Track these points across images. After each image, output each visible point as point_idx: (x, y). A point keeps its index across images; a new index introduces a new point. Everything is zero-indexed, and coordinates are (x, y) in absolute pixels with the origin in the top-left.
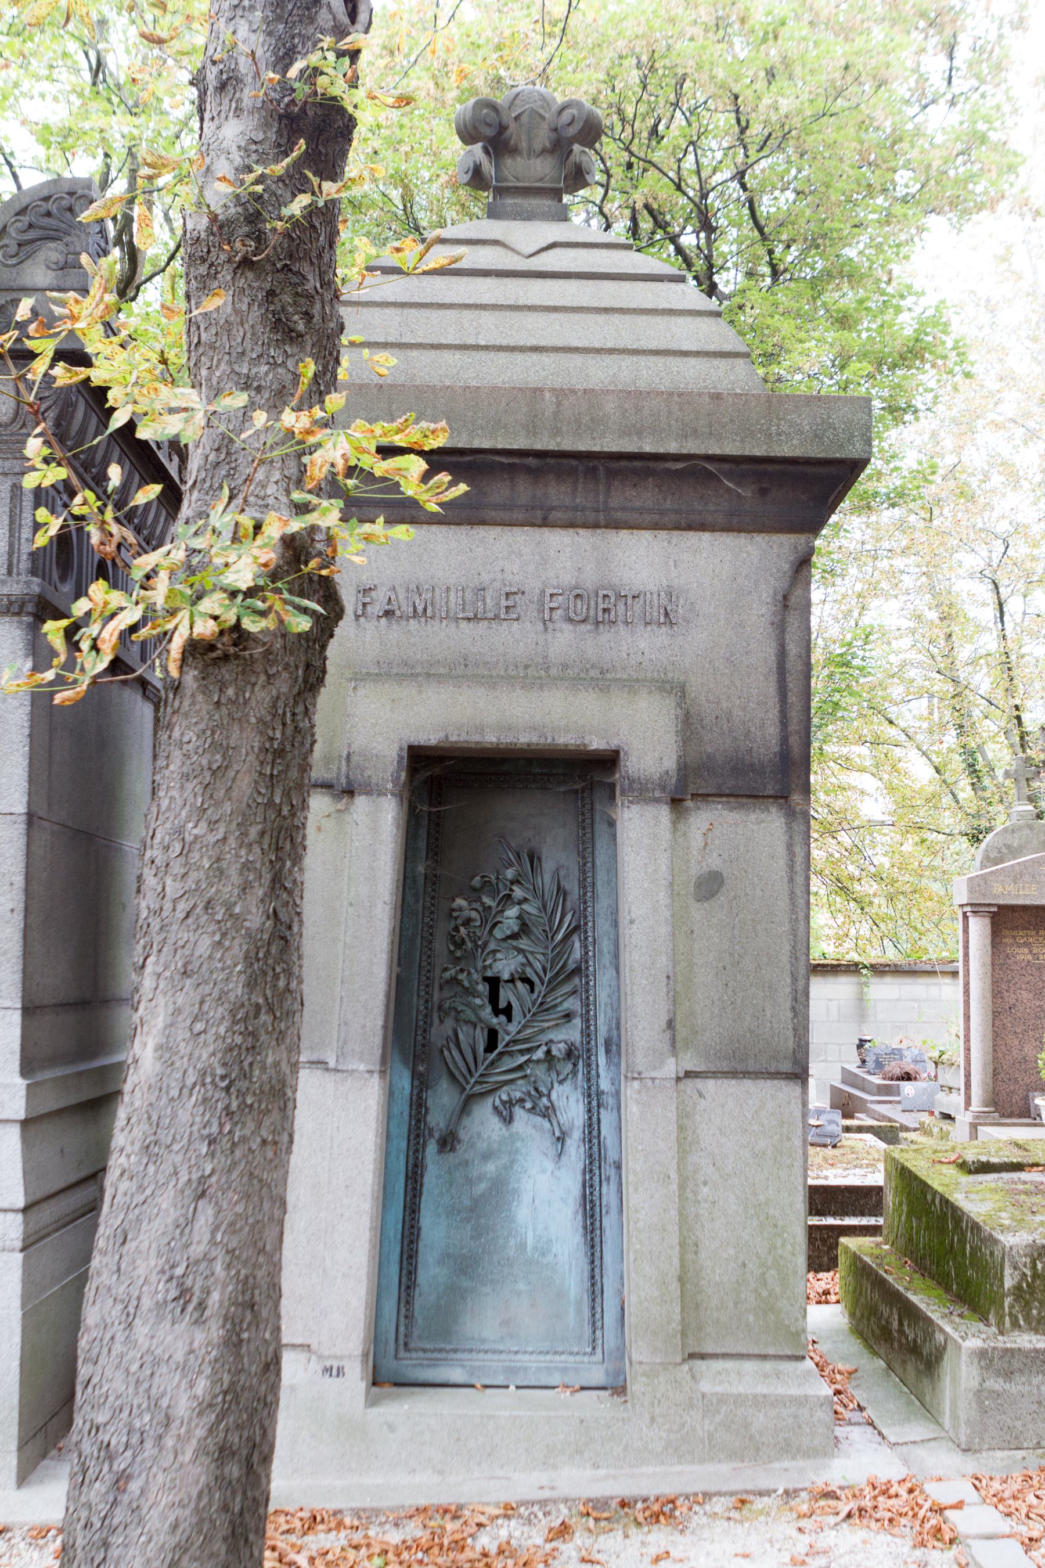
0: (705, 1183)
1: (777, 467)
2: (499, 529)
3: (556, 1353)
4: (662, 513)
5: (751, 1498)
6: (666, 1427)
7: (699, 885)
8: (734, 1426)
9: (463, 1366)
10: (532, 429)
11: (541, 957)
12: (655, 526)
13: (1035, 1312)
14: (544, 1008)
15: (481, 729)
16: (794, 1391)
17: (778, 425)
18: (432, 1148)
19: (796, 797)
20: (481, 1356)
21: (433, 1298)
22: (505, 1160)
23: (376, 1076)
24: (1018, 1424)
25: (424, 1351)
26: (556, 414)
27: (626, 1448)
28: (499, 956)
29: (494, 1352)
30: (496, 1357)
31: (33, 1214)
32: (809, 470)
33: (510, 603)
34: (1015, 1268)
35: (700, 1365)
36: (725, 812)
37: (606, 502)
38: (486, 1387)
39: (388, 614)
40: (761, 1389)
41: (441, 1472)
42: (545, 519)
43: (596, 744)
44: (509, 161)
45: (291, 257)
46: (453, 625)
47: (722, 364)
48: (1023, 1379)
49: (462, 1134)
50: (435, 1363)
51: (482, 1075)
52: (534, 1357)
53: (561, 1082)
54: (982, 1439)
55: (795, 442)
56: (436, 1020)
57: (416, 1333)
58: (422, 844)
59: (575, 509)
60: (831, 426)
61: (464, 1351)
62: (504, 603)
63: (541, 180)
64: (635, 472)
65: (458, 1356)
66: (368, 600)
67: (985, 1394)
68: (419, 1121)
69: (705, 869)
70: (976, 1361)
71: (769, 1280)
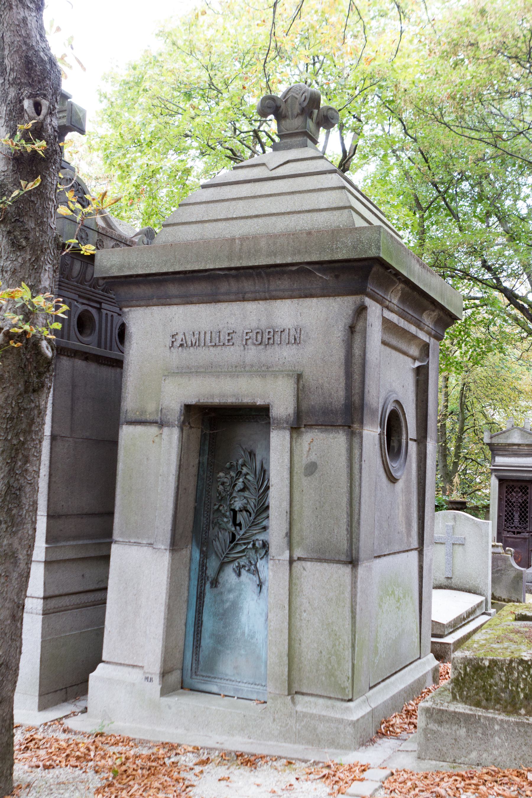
0: (305, 611)
1: (339, 264)
2: (227, 303)
3: (255, 684)
4: (293, 290)
5: (294, 762)
6: (280, 724)
7: (306, 469)
8: (309, 729)
9: (217, 685)
10: (230, 258)
11: (254, 501)
12: (291, 297)
13: (465, 693)
14: (254, 524)
15: (212, 396)
16: (338, 716)
17: (337, 244)
18: (208, 585)
19: (356, 426)
20: (225, 682)
21: (207, 653)
22: (237, 593)
23: (168, 551)
24: (444, 749)
25: (203, 676)
26: (240, 249)
27: (262, 731)
28: (236, 499)
29: (231, 680)
30: (231, 683)
31: (49, 601)
32: (355, 264)
33: (230, 338)
34: (455, 669)
35: (299, 698)
36: (319, 434)
37: (268, 287)
38: (226, 696)
39: (181, 345)
40: (324, 713)
41: (188, 730)
42: (243, 298)
43: (259, 402)
44: (283, 122)
45: (19, 216)
46: (207, 349)
47: (337, 213)
48: (448, 726)
49: (220, 580)
50: (206, 682)
51: (227, 554)
52: (246, 685)
53: (261, 558)
54: (426, 753)
55: (344, 252)
56: (211, 528)
57: (200, 668)
58: (206, 448)
59: (255, 292)
60: (361, 242)
61: (218, 678)
62: (227, 338)
63: (297, 129)
64: (277, 272)
65: (216, 680)
66: (174, 340)
67: (428, 731)
68: (203, 573)
69: (309, 461)
70: (424, 713)
71: (332, 661)
